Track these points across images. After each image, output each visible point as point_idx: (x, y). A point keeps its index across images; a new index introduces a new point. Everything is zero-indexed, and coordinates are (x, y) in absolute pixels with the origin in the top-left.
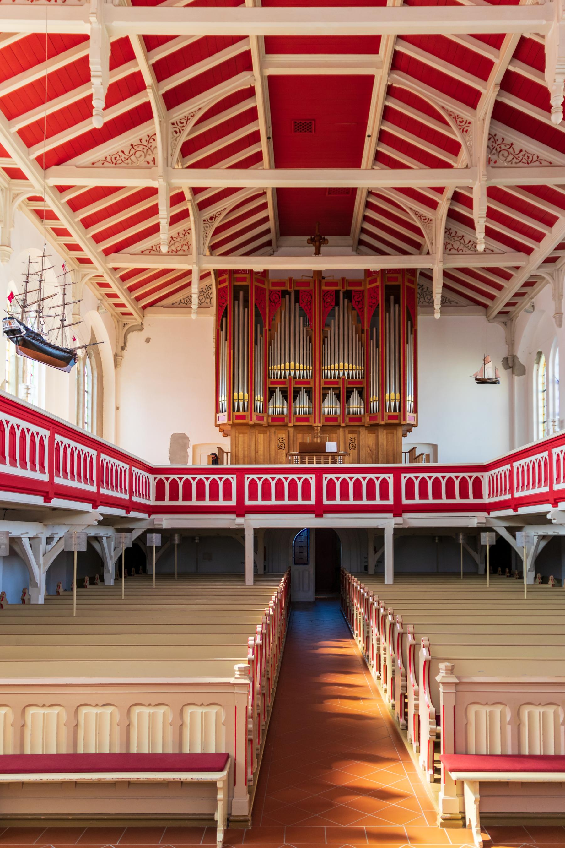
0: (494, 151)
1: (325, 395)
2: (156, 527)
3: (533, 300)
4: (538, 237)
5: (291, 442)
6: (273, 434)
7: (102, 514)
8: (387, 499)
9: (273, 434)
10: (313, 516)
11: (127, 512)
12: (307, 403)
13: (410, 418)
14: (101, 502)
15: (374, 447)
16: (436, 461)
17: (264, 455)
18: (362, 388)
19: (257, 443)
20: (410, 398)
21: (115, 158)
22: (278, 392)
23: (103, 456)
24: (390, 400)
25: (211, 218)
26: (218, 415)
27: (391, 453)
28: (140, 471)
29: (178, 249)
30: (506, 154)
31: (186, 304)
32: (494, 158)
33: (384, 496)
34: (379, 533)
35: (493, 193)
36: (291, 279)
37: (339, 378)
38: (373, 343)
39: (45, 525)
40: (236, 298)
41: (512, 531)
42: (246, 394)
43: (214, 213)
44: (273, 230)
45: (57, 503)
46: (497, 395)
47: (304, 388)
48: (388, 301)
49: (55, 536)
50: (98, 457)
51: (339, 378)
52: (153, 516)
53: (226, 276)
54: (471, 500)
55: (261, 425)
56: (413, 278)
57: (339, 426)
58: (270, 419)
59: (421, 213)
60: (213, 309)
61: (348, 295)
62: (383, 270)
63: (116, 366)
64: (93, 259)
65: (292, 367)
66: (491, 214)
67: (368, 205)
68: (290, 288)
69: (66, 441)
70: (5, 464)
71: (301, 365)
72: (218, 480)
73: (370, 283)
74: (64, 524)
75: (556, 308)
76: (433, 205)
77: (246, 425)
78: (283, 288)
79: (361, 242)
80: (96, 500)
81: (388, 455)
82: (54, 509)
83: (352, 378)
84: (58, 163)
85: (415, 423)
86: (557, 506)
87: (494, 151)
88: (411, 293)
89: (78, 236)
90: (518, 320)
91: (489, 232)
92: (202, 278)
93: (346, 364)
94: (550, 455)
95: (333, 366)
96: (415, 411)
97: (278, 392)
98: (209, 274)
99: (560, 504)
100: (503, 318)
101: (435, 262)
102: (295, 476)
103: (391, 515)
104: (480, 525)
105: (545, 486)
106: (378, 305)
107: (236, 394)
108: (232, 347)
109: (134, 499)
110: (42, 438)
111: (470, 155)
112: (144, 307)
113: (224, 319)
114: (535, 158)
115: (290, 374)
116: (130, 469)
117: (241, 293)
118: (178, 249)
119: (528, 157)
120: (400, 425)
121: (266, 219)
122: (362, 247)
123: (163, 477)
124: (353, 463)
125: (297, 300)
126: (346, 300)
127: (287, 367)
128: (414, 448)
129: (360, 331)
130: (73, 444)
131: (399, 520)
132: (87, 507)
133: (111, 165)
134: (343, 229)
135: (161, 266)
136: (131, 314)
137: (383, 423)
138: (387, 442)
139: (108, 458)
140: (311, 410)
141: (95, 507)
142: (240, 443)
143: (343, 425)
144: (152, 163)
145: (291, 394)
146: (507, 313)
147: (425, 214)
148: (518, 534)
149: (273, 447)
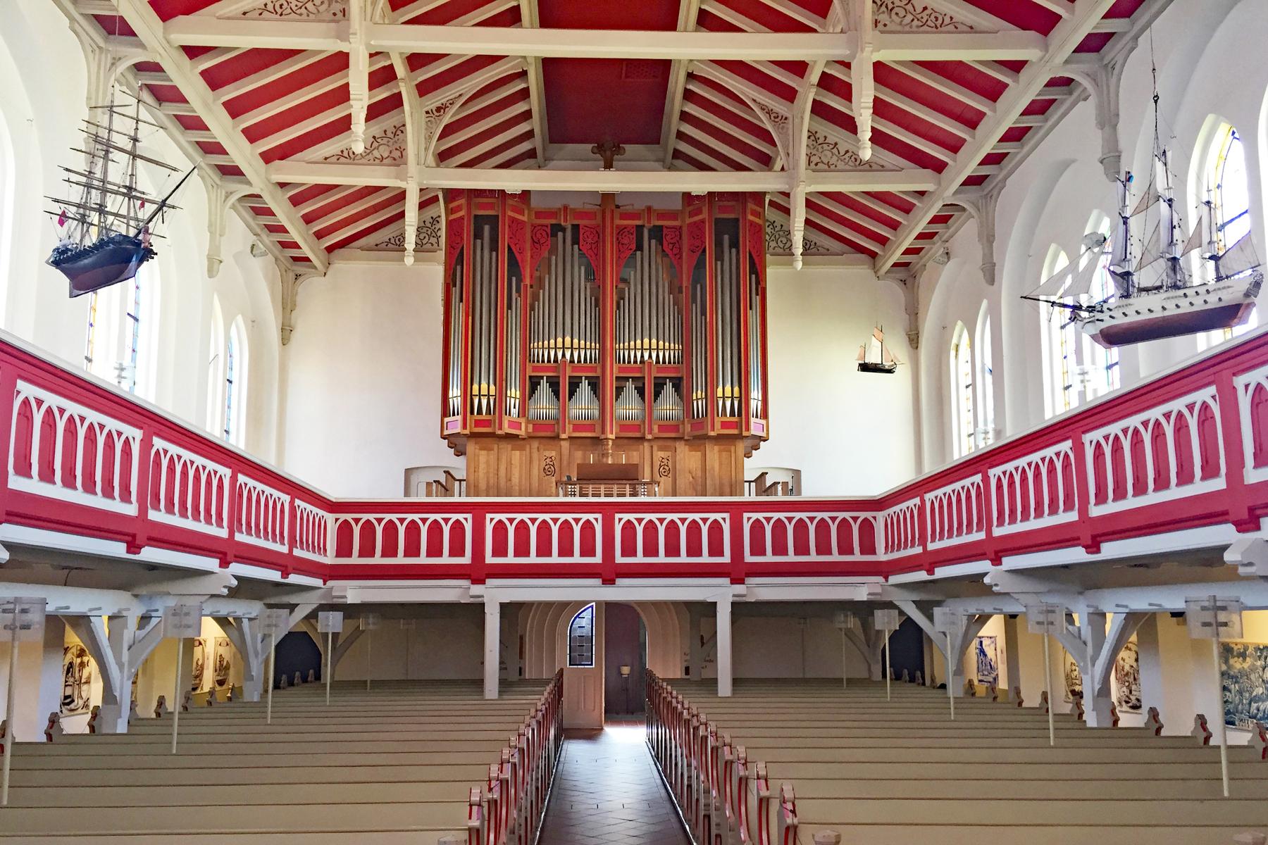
0: (883, 8)
1: (619, 390)
2: (336, 601)
3: (947, 245)
4: (954, 146)
5: (565, 463)
6: (535, 451)
7: (236, 577)
8: (721, 554)
9: (535, 451)
10: (598, 581)
11: (285, 575)
12: (591, 402)
13: (756, 426)
14: (8, 514)
15: (699, 473)
16: (799, 493)
17: (520, 485)
18: (680, 379)
19: (510, 463)
20: (756, 394)
21: (281, 6)
22: (544, 385)
23: (242, 478)
24: (724, 397)
25: (438, 109)
26: (446, 420)
27: (726, 482)
28: (309, 507)
29: (385, 155)
30: (902, 13)
31: (397, 245)
32: (884, 18)
33: (716, 550)
34: (710, 609)
35: (882, 73)
36: (566, 208)
37: (642, 362)
38: (696, 309)
39: (136, 596)
40: (478, 235)
41: (926, 608)
42: (492, 387)
43: (444, 101)
44: (537, 131)
45: (150, 554)
46: (895, 387)
47: (586, 378)
48: (719, 244)
49: (154, 614)
50: (234, 479)
51: (642, 362)
52: (330, 583)
53: (462, 201)
54: (857, 557)
55: (517, 436)
56: (758, 209)
57: (643, 439)
58: (531, 426)
59: (771, 107)
60: (441, 255)
61: (657, 233)
62: (711, 194)
63: (285, 341)
64: (244, 168)
65: (568, 347)
66: (880, 108)
67: (689, 96)
68: (566, 220)
69: (174, 450)
70: (54, 483)
71: (582, 342)
72: (442, 522)
73: (691, 215)
74: (169, 594)
75: (984, 255)
76: (789, 94)
77: (492, 435)
78: (553, 221)
79: (677, 154)
80: (225, 553)
81: (721, 485)
82: (152, 567)
83: (664, 362)
84: (188, 11)
85: (764, 434)
86: (1000, 564)
87: (883, 8)
88: (757, 231)
89: (223, 129)
90: (923, 279)
91: (878, 138)
92: (422, 206)
93: (654, 341)
94: (986, 479)
95: (632, 343)
96: (765, 415)
97: (544, 385)
98: (436, 199)
99: (1004, 560)
100: (901, 273)
101: (798, 180)
102: (569, 517)
103: (727, 581)
104: (872, 597)
105: (979, 530)
106: (704, 251)
107: (476, 387)
108: (470, 312)
109: (297, 552)
110: (127, 441)
111: (847, 13)
112: (330, 249)
113: (459, 268)
114: (947, 20)
115: (564, 355)
116: (292, 503)
117: (487, 228)
118: (385, 155)
119: (937, 19)
120: (740, 437)
121: (527, 115)
122: (680, 160)
123: (349, 517)
124: (666, 495)
125: (575, 241)
126: (653, 242)
127: (560, 344)
128: (764, 474)
129: (675, 289)
130: (199, 460)
131: (739, 589)
132: (211, 564)
133: (274, 16)
134: (650, 133)
135: (246, 42)
136: (307, 259)
137: (712, 434)
138: (721, 464)
139: (251, 483)
140: (597, 413)
141: (224, 564)
142: (482, 466)
143: (649, 437)
144: (340, 15)
145: (565, 387)
146: (907, 265)
147: (776, 110)
148: (937, 611)
149: (535, 472)
